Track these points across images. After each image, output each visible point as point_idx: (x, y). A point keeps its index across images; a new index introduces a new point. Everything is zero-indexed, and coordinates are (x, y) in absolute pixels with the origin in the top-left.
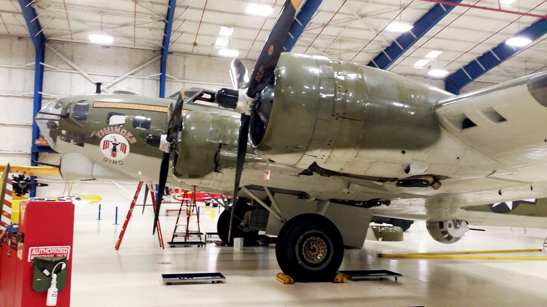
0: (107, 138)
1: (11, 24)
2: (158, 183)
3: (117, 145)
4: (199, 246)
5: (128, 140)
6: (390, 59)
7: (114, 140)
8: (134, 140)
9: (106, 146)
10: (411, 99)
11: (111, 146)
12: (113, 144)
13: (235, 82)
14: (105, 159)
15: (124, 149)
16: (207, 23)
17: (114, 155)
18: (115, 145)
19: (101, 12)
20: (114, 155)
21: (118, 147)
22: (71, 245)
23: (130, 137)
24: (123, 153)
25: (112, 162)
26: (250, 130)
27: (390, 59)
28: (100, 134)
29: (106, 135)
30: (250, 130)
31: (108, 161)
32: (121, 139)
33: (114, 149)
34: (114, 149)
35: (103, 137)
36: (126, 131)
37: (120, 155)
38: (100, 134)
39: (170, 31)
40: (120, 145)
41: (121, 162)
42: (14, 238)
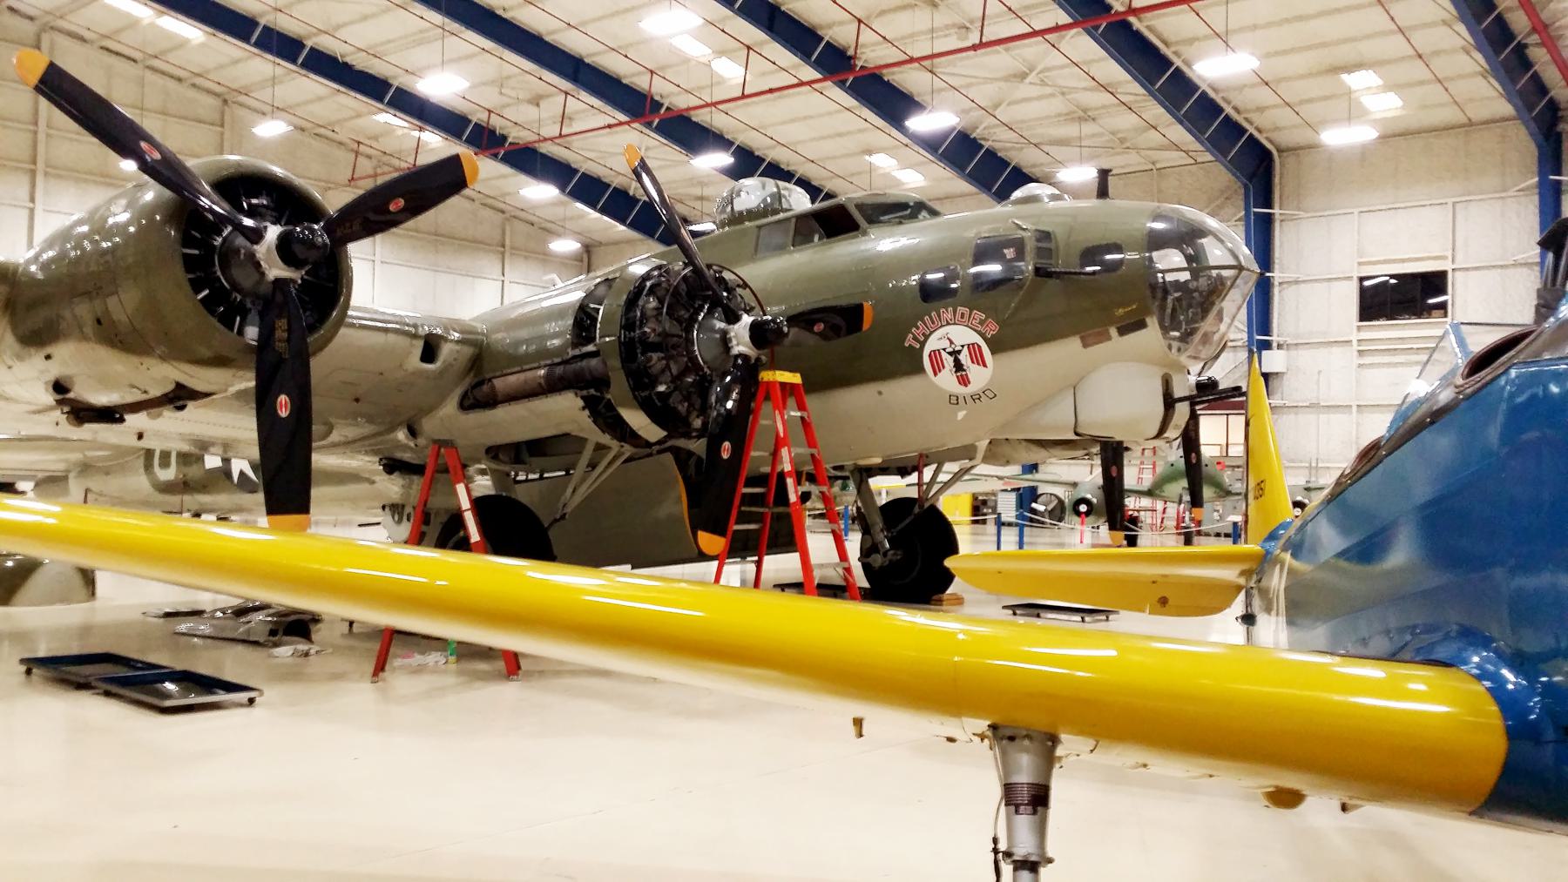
0: (933, 344)
2: (1073, 345)
5: (979, 333)
6: (300, 60)
8: (992, 329)
9: (938, 367)
10: (137, 232)
11: (949, 361)
17: (964, 381)
18: (955, 354)
19: (512, 664)
20: (964, 381)
21: (964, 357)
22: (870, 596)
23: (982, 323)
24: (981, 368)
25: (969, 400)
27: (300, 60)
28: (915, 338)
29: (927, 337)
32: (962, 335)
33: (958, 366)
34: (958, 366)
35: (923, 344)
36: (966, 310)
37: (979, 376)
38: (915, 338)
42: (1358, 81)
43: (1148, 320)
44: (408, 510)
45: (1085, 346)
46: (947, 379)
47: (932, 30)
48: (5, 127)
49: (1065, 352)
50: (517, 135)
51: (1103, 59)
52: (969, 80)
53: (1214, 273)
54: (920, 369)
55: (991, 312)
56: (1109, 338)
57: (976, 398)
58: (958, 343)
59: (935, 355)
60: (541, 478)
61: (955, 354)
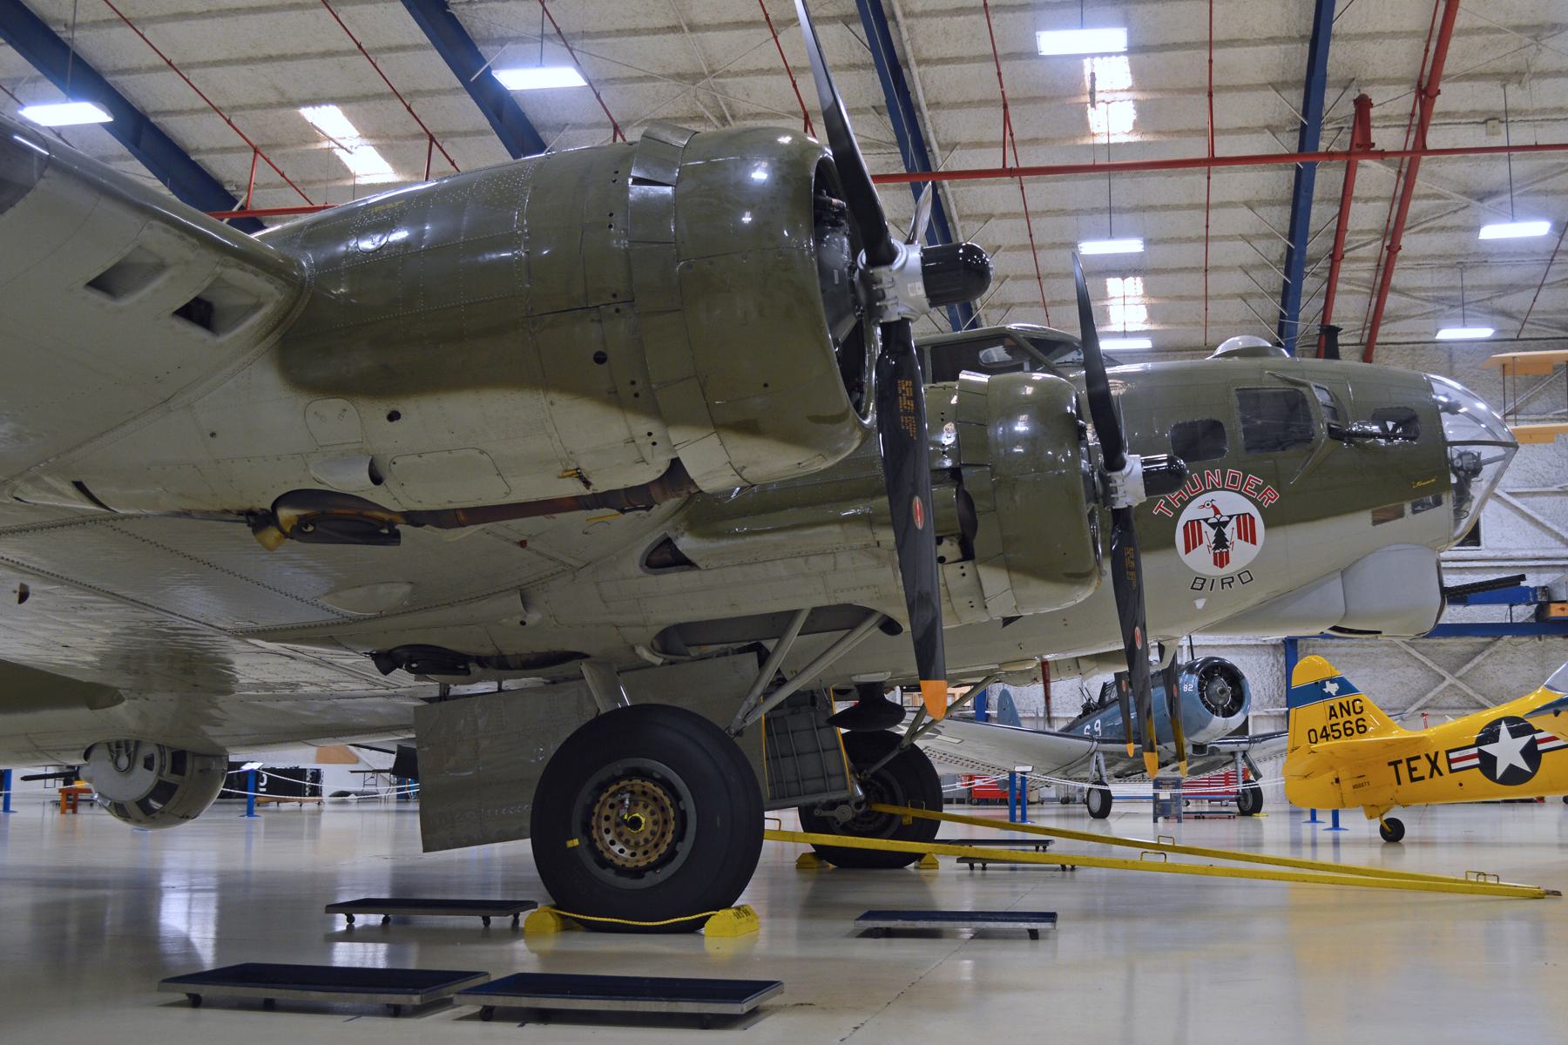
1: (1082, 816)
3: (1225, 524)
4: (1557, 714)
5: (1254, 501)
7: (1211, 513)
8: (1271, 497)
9: (1192, 541)
11: (1209, 534)
12: (1213, 525)
13: (1009, 306)
14: (1200, 584)
15: (1248, 534)
16: (1189, 240)
17: (1221, 560)
18: (1219, 526)
20: (1221, 560)
21: (1230, 532)
23: (1258, 489)
24: (1249, 545)
25: (1218, 584)
26: (494, 256)
28: (1168, 504)
29: (1185, 504)
30: (494, 256)
31: (1208, 584)
32: (1232, 503)
33: (1221, 541)
34: (1221, 541)
37: (1242, 553)
38: (1168, 504)
39: (1306, 234)
40: (1233, 523)
41: (1245, 577)
43: (1444, 497)
44: (146, 751)
45: (1375, 522)
46: (1201, 560)
47: (1211, 44)
48: (1561, 109)
49: (1351, 530)
50: (977, 98)
51: (418, 47)
52: (1551, 184)
53: (51, 771)
54: (1171, 544)
55: (1274, 478)
56: (1401, 515)
57: (1227, 582)
58: (1225, 511)
59: (1193, 529)
60: (500, 690)
61: (1219, 526)
